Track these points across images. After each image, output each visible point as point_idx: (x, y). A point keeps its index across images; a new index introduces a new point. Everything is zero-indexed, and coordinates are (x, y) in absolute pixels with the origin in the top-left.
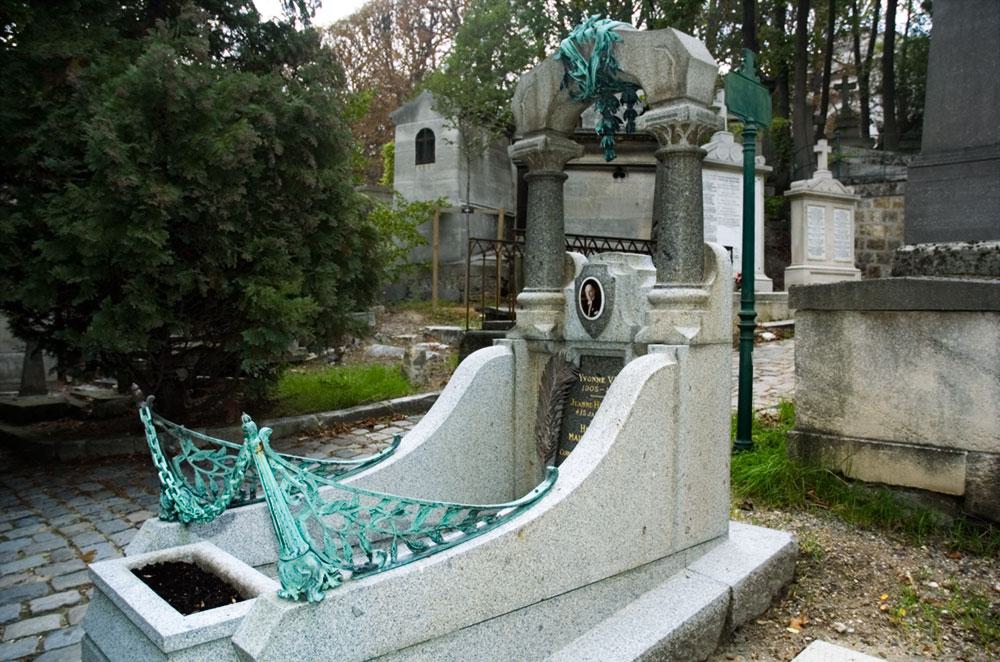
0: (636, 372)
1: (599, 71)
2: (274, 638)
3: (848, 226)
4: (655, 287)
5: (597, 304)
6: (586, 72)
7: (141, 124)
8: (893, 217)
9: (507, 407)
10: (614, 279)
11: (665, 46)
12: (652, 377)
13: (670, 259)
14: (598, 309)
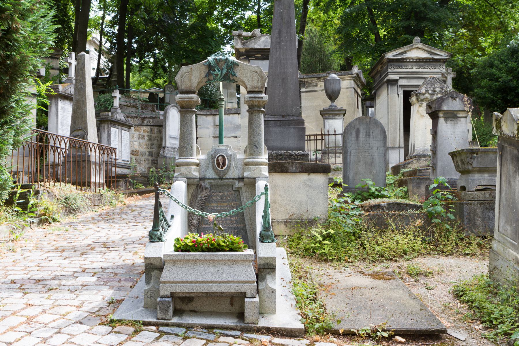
5: (224, 164)
7: (26, 81)
8: (143, 138)
11: (257, 72)
13: (257, 148)
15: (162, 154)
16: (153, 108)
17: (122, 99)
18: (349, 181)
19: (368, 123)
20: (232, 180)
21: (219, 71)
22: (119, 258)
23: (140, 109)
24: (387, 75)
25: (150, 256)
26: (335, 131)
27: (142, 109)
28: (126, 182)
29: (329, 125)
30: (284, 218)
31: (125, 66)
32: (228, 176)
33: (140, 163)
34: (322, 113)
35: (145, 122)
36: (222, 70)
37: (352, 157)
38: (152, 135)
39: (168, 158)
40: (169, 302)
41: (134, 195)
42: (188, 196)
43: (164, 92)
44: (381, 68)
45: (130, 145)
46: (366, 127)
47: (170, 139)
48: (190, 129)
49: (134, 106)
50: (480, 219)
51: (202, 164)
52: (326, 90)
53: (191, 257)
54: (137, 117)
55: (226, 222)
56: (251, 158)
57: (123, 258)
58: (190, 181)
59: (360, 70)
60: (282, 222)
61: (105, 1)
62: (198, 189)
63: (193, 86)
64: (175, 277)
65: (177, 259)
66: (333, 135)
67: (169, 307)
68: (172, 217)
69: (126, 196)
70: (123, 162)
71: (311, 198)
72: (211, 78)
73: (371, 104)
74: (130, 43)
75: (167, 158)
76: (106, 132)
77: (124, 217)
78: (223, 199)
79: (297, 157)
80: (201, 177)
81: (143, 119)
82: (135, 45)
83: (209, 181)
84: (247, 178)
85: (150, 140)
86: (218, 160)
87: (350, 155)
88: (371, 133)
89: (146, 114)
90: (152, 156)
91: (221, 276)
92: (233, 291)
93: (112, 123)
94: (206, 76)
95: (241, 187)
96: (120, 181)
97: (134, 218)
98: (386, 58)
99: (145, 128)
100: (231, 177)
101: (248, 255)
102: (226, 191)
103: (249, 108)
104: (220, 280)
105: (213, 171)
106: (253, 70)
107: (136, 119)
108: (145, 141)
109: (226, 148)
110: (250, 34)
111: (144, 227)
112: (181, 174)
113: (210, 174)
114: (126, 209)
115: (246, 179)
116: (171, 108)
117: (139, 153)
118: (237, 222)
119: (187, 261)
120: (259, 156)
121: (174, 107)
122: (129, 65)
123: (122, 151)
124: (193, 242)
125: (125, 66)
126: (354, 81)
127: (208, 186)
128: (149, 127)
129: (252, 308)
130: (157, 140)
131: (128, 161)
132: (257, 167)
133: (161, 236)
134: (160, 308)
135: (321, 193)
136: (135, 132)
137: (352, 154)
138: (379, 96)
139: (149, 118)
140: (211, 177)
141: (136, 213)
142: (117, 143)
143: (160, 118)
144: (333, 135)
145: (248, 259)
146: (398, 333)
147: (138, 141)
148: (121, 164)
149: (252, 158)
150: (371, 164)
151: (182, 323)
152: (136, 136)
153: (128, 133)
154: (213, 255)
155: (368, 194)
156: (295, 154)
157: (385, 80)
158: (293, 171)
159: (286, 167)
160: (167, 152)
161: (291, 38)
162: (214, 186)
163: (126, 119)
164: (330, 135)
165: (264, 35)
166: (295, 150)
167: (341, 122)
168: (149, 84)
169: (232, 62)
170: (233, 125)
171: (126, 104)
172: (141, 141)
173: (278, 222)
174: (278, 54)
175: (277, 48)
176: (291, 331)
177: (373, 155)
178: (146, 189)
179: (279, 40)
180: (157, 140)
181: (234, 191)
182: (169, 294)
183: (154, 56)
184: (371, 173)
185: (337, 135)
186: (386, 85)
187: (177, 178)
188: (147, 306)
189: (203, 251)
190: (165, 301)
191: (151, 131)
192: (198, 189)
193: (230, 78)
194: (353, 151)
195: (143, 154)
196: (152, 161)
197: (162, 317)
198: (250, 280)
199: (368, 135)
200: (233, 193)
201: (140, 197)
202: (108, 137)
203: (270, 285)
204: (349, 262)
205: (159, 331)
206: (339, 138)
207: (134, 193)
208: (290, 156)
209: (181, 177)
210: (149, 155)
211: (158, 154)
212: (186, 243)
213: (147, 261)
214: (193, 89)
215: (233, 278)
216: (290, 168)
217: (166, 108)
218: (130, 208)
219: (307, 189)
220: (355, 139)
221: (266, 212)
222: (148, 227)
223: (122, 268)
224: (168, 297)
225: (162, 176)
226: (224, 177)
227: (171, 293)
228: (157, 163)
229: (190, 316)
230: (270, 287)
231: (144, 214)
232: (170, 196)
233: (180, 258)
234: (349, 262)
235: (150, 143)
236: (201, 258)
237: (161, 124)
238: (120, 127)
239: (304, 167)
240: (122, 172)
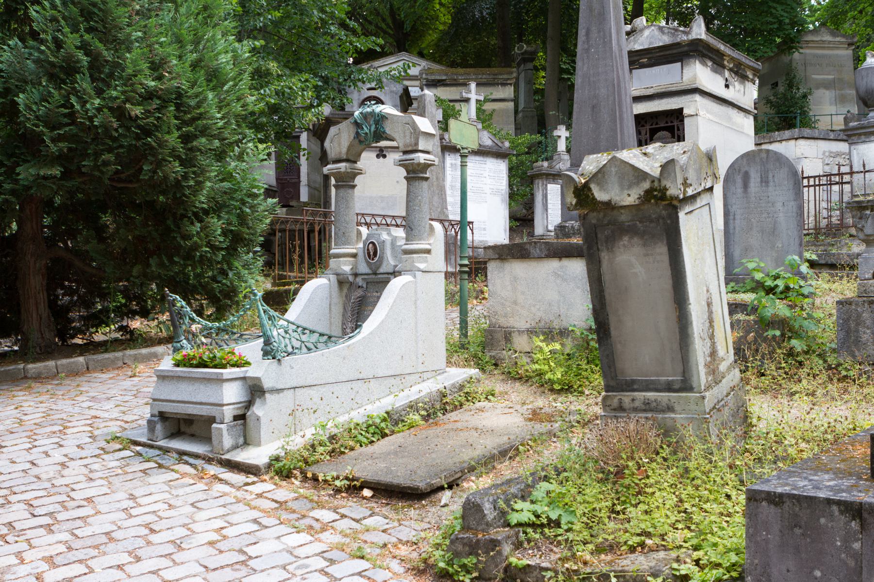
0: (395, 284)
1: (375, 132)
2: (266, 370)
3: (753, 191)
4: (405, 244)
6: (368, 132)
9: (327, 311)
12: (404, 285)
13: (412, 230)
18: (733, 264)
20: (386, 276)
26: (864, 166)
30: (528, 326)
32: (381, 270)
36: (370, 126)
37: (737, 222)
50: (868, 331)
60: (524, 331)
76: (541, 192)
83: (363, 277)
87: (734, 219)
93: (551, 177)
100: (385, 271)
103: (408, 172)
113: (363, 268)
135: (578, 288)
137: (738, 217)
146: (365, 485)
150: (774, 231)
158: (536, 255)
159: (527, 249)
161: (604, 40)
164: (854, 173)
173: (519, 331)
174: (585, 69)
177: (775, 216)
179: (586, 46)
184: (773, 247)
194: (739, 212)
199: (765, 182)
202: (543, 200)
236: (182, 375)
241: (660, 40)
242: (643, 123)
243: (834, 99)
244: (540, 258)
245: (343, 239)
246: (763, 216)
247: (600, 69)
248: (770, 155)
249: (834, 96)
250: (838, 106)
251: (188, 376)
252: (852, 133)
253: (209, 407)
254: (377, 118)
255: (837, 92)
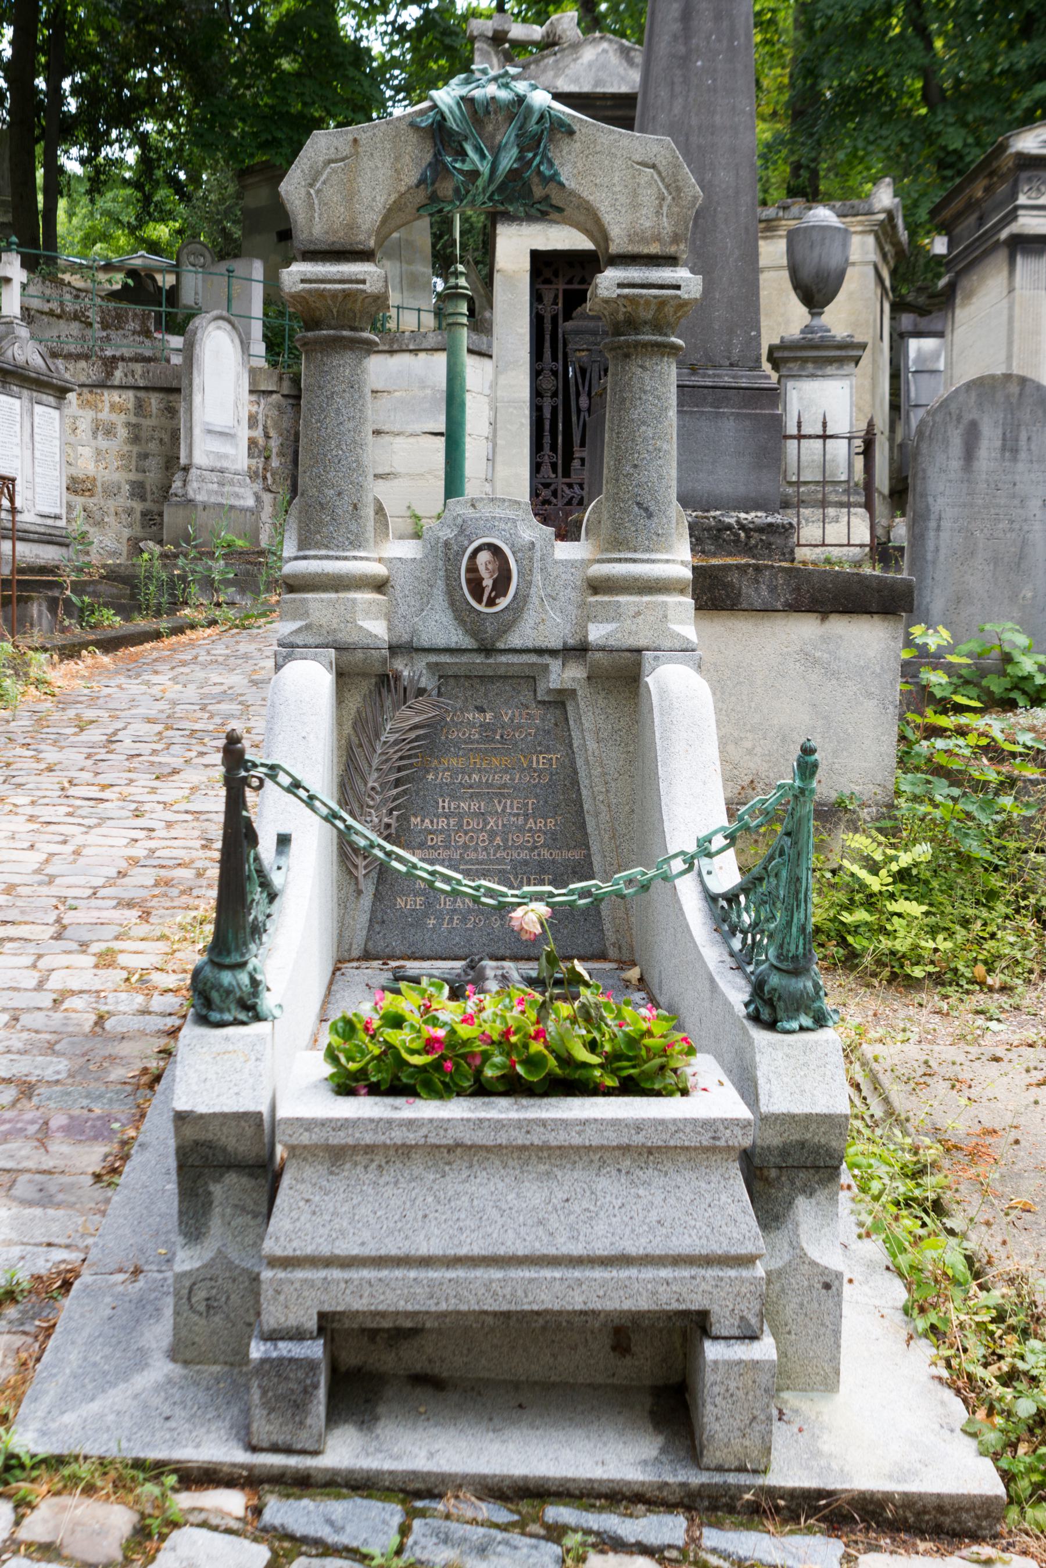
6: (484, 168)
8: (109, 431)
10: (533, 543)
11: (654, 166)
13: (650, 516)
14: (505, 595)
15: (180, 492)
16: (143, 323)
17: (32, 290)
19: (1014, 400)
20: (534, 659)
21: (483, 157)
22: (33, 983)
23: (97, 326)
24: (1012, 216)
25: (202, 1109)
26: (825, 425)
27: (104, 329)
28: (53, 605)
29: (800, 399)
31: (40, 173)
32: (515, 640)
33: (99, 524)
34: (776, 355)
35: (118, 374)
36: (497, 152)
37: (945, 535)
38: (142, 421)
39: (200, 508)
40: (311, 1365)
41: (84, 652)
42: (339, 723)
43: (176, 270)
44: (987, 190)
45: (64, 459)
46: (1005, 418)
47: (209, 437)
48: (350, 425)
49: (76, 317)
51: (401, 583)
52: (794, 270)
53: (424, 1131)
54: (86, 357)
55: (505, 840)
56: (619, 560)
57: (55, 982)
58: (347, 657)
59: (897, 200)
61: (3, 224)
62: (384, 692)
63: (364, 227)
64: (343, 1233)
65: (350, 1141)
66: (818, 437)
67: (308, 1391)
68: (283, 841)
69: (56, 657)
70: (39, 520)
71: (825, 718)
72: (446, 189)
73: (916, 325)
74: (56, 94)
75: (195, 506)
77: (51, 755)
78: (493, 741)
79: (748, 537)
80: (394, 641)
81: (111, 363)
82: (72, 105)
83: (433, 658)
84: (602, 649)
85: (135, 439)
86: (472, 569)
87: (938, 529)
88: (1023, 442)
89: (118, 347)
90: (143, 499)
91: (585, 1229)
92: (644, 1304)
94: (422, 182)
95: (575, 686)
96: (29, 599)
97: (90, 762)
98: (1012, 150)
99: (115, 397)
100: (530, 645)
101: (723, 1121)
102: (506, 703)
104: (577, 1249)
105: (449, 613)
106: (637, 157)
107: (83, 364)
108: (118, 444)
109: (510, 514)
110: (537, 32)
111: (133, 806)
112: (308, 627)
114: (56, 716)
115: (599, 655)
116: (212, 326)
117: (95, 486)
118: (554, 840)
119: (405, 1151)
120: (657, 551)
121: (221, 323)
122: (55, 171)
123: (37, 480)
124: (431, 1045)
125: (40, 173)
126: (877, 239)
127: (427, 681)
128: (130, 394)
129: (740, 1394)
130: (161, 440)
131: (57, 517)
132: (646, 599)
133: (255, 994)
134: (264, 1393)
135: (869, 695)
136: (81, 412)
137: (946, 524)
138: (969, 296)
139: (131, 360)
140: (441, 641)
141: (94, 735)
142: (17, 451)
143: (168, 361)
144: (818, 437)
145: (722, 1143)
147: (93, 443)
148: (33, 528)
149: (626, 560)
151: (379, 1473)
152: (85, 425)
153: (56, 414)
154: (543, 1123)
155: (1006, 682)
156: (738, 522)
157: (1004, 235)
159: (731, 585)
160: (195, 485)
161: (731, 40)
162: (452, 681)
163: (49, 361)
164: (805, 437)
165: (594, 39)
166: (737, 508)
167: (847, 390)
168: (122, 241)
169: (542, 117)
170: (429, 392)
171: (46, 307)
172: (102, 443)
174: (677, 109)
175: (673, 83)
176: (940, 1509)
177: (1026, 528)
178: (129, 628)
179: (682, 49)
180: (161, 440)
181: (543, 703)
182: (312, 1324)
183: (142, 139)
185: (831, 437)
186: (1002, 255)
187: (293, 646)
188: (188, 1355)
189: (482, 1090)
190: (291, 1360)
191: (140, 407)
192: (384, 692)
193: (531, 191)
194: (949, 513)
195: (111, 491)
196: (144, 514)
197: (274, 1438)
198: (733, 1251)
199: (1012, 450)
200: (536, 712)
201: (106, 659)
203: (814, 1253)
204: (991, 989)
205: (265, 1529)
206: (839, 449)
207: (85, 645)
208: (719, 530)
209: (310, 640)
210: (132, 495)
211: (165, 489)
212: (390, 1046)
213: (191, 1133)
214: (362, 237)
215: (643, 1241)
216: (747, 590)
217: (191, 326)
218: (71, 713)
219: (814, 677)
220: (962, 462)
221: (798, 879)
222: (146, 807)
223: (51, 1048)
224: (298, 1335)
225: (183, 578)
226: (501, 645)
227: (322, 1316)
228: (161, 524)
229: (414, 1415)
230: (814, 1264)
231: (127, 745)
232: (302, 793)
233: (368, 1139)
234: (991, 989)
235: (135, 449)
237: (175, 384)
238: (26, 393)
239: (805, 587)
240: (37, 557)
241: (623, 79)
242: (548, 273)
243: (398, 279)
244: (767, 610)
245: (353, 527)
246: (1001, 526)
247: (718, 118)
248: (1028, 390)
249: (398, 272)
250: (405, 293)
251: (520, 1139)
252: (792, 354)
253: (665, 1273)
254: (532, 126)
255: (405, 266)
